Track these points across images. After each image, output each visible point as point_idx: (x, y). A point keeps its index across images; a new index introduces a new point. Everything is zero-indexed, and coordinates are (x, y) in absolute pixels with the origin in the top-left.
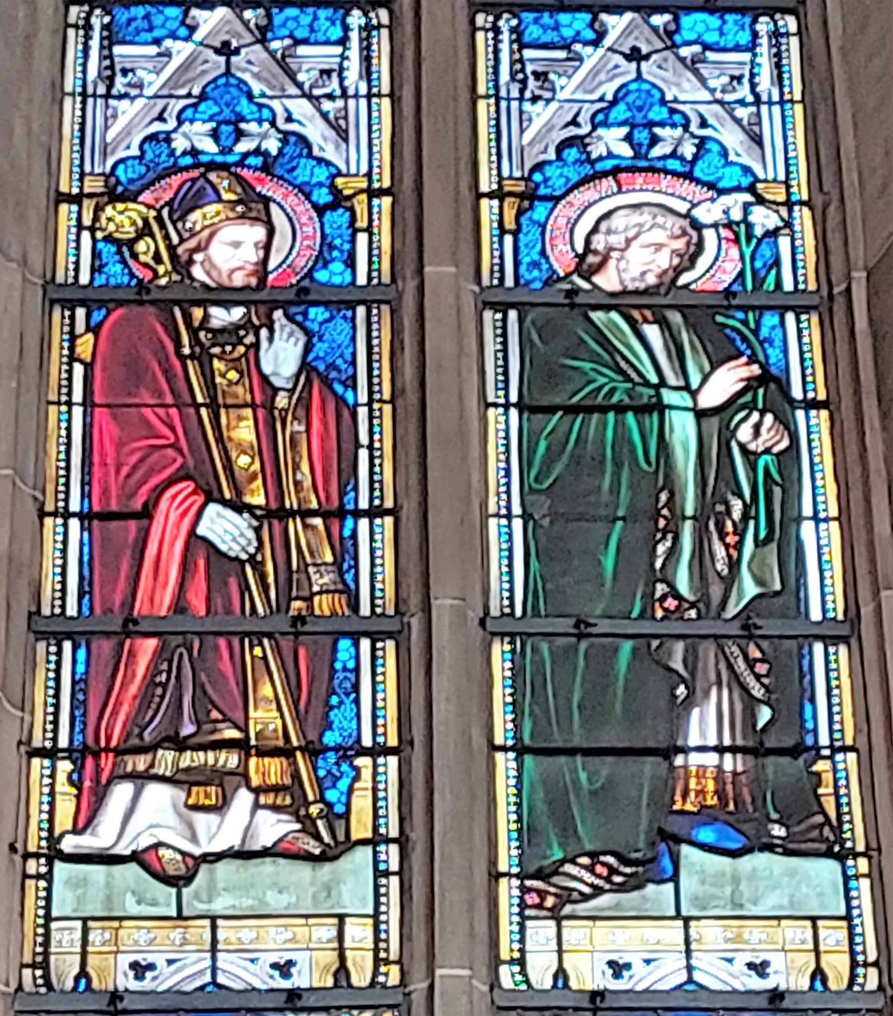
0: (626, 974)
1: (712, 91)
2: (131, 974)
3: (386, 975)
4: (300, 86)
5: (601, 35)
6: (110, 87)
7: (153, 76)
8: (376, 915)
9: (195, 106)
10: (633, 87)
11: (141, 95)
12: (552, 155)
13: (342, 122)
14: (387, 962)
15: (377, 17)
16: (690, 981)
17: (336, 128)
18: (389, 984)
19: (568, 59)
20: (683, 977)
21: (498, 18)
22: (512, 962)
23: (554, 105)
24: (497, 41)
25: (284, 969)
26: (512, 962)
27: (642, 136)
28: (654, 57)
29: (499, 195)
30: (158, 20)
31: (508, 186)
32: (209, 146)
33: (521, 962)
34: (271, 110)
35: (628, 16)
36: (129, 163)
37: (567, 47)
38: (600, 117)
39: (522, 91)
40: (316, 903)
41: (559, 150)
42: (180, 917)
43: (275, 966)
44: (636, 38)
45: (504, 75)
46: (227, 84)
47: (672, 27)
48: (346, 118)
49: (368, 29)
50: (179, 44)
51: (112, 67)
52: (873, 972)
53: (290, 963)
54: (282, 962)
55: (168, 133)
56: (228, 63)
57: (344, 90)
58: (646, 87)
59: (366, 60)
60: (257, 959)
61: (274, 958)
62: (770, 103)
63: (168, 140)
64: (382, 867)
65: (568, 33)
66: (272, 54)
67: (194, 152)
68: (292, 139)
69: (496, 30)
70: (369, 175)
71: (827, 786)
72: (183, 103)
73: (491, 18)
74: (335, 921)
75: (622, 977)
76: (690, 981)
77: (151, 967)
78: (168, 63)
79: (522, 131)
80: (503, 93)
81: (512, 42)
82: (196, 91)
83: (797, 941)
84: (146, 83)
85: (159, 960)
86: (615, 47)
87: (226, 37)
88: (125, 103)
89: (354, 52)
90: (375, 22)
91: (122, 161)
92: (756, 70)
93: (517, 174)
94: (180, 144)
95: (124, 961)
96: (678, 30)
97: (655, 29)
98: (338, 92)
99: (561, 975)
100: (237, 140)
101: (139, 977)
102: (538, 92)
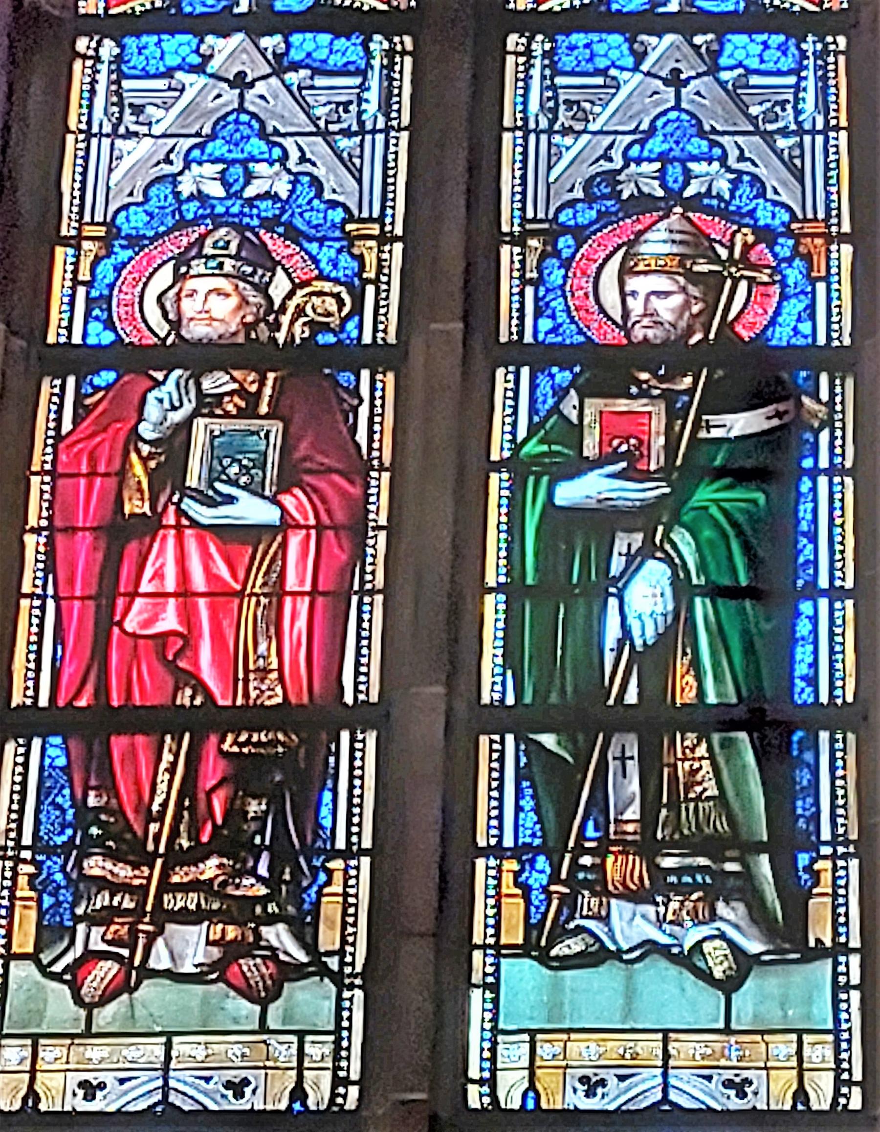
0: (99, 1094)
1: (753, 120)
2: (81, 1093)
3: (345, 1097)
4: (314, 120)
5: (640, 57)
6: (552, 122)
7: (161, 113)
8: (836, 1031)
9: (201, 146)
10: (673, 115)
11: (585, 131)
12: (579, 193)
13: (797, 162)
14: (850, 1083)
15: (402, 43)
16: (665, 1099)
17: (789, 165)
18: (346, 1107)
19: (605, 86)
20: (158, 1097)
21: (530, 40)
22: (481, 1082)
23: (585, 138)
24: (528, 66)
25: (238, 1088)
26: (481, 1082)
27: (674, 172)
28: (693, 83)
29: (519, 240)
30: (600, 49)
31: (88, 231)
32: (216, 190)
33: (492, 1082)
34: (721, 146)
35: (238, 37)
36: (132, 209)
37: (603, 72)
38: (635, 151)
39: (552, 122)
40: (624, 1021)
41: (588, 185)
42: (169, 1035)
43: (228, 1085)
44: (677, 61)
45: (534, 106)
46: (237, 122)
47: (715, 47)
48: (802, 156)
49: (390, 53)
50: (626, 75)
51: (120, 104)
52: (856, 1092)
53: (246, 1082)
54: (237, 1080)
55: (175, 176)
56: (241, 96)
57: (361, 123)
58: (244, 118)
59: (823, 91)
60: (211, 1078)
61: (229, 1075)
62: (374, 131)
63: (175, 184)
64: (842, 979)
65: (172, 61)
66: (722, 84)
67: (200, 196)
68: (746, 178)
69: (528, 53)
70: (381, 220)
71: (826, 886)
72: (629, 139)
73: (93, 44)
74: (294, 1038)
75: (595, 1095)
76: (665, 1099)
77: (102, 1086)
78: (614, 95)
79: (110, 170)
80: (532, 125)
81: (544, 67)
82: (644, 126)
83: (628, 1056)
84: (154, 120)
85: (109, 1078)
86: (653, 71)
87: (241, 68)
88: (568, 140)
89: (374, 82)
90: (399, 48)
91: (126, 207)
92: (801, 95)
93: (99, 218)
94: (186, 187)
95: (74, 1079)
96: (719, 53)
97: (696, 48)
98: (355, 128)
99: (531, 1094)
100: (247, 183)
101: (90, 1096)
102: (133, 128)
